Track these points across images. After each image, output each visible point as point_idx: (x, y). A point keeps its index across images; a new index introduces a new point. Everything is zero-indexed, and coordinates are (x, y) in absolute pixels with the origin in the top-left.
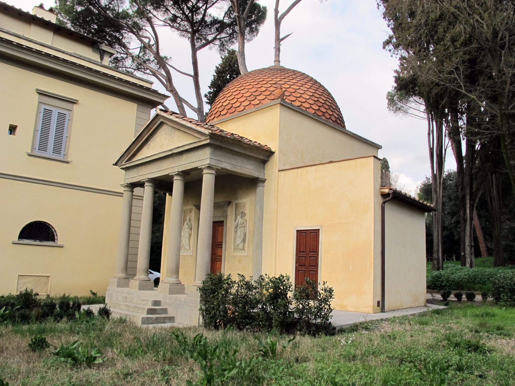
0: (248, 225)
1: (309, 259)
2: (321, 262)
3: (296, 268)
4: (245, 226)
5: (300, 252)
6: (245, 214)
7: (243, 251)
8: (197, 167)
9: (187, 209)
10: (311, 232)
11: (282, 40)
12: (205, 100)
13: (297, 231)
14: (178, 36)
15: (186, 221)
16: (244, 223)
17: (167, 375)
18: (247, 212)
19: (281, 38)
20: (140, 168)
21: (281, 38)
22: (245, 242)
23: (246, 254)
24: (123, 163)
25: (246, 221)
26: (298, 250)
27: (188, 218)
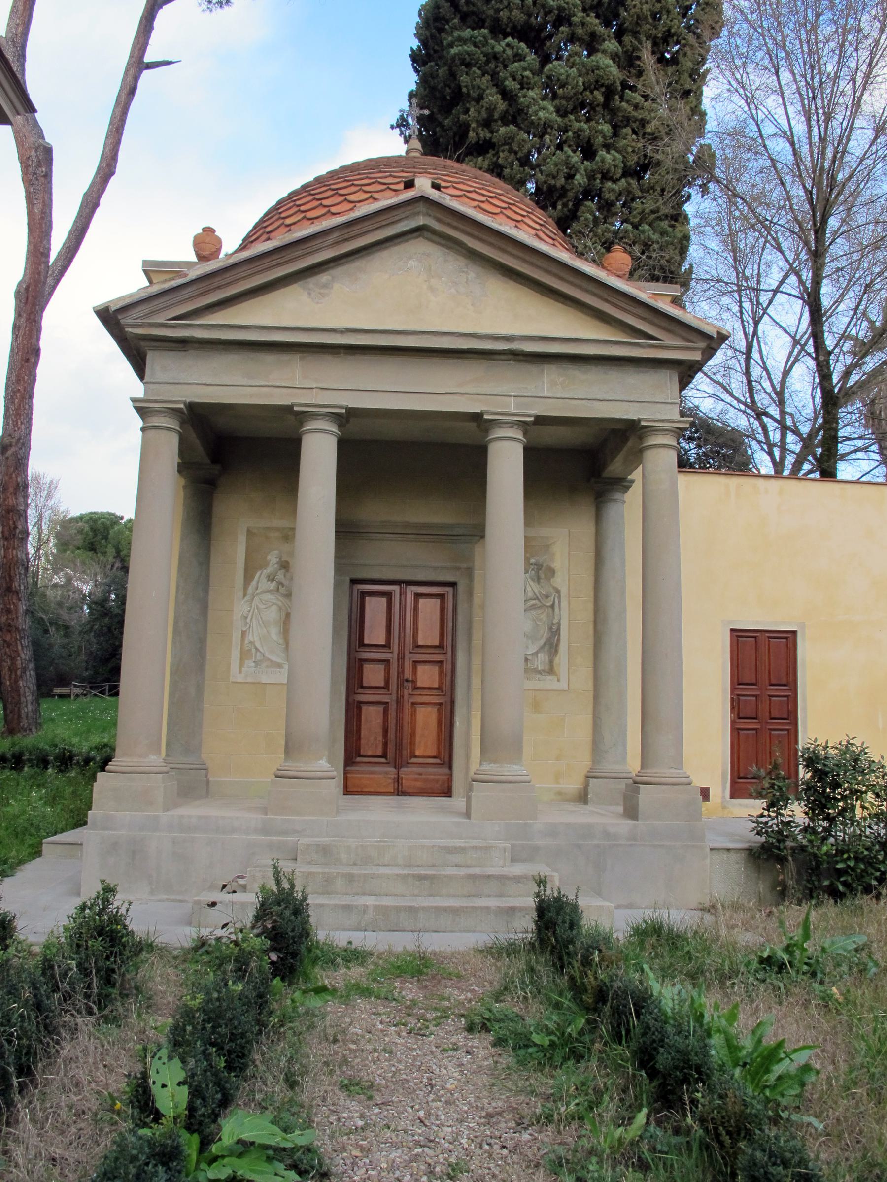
0: (564, 603)
1: (768, 702)
2: (805, 709)
3: (733, 722)
4: (552, 606)
5: (739, 684)
6: (552, 572)
7: (549, 677)
8: (639, 420)
9: (268, 529)
10: (769, 637)
11: (150, 66)
12: (644, 292)
13: (732, 630)
14: (410, 90)
15: (265, 565)
16: (547, 597)
17: (826, 774)
18: (557, 565)
19: (147, 59)
20: (285, 357)
21: (147, 59)
22: (556, 651)
23: (563, 685)
24: (160, 319)
25: (558, 592)
26: (735, 681)
27: (273, 559)
